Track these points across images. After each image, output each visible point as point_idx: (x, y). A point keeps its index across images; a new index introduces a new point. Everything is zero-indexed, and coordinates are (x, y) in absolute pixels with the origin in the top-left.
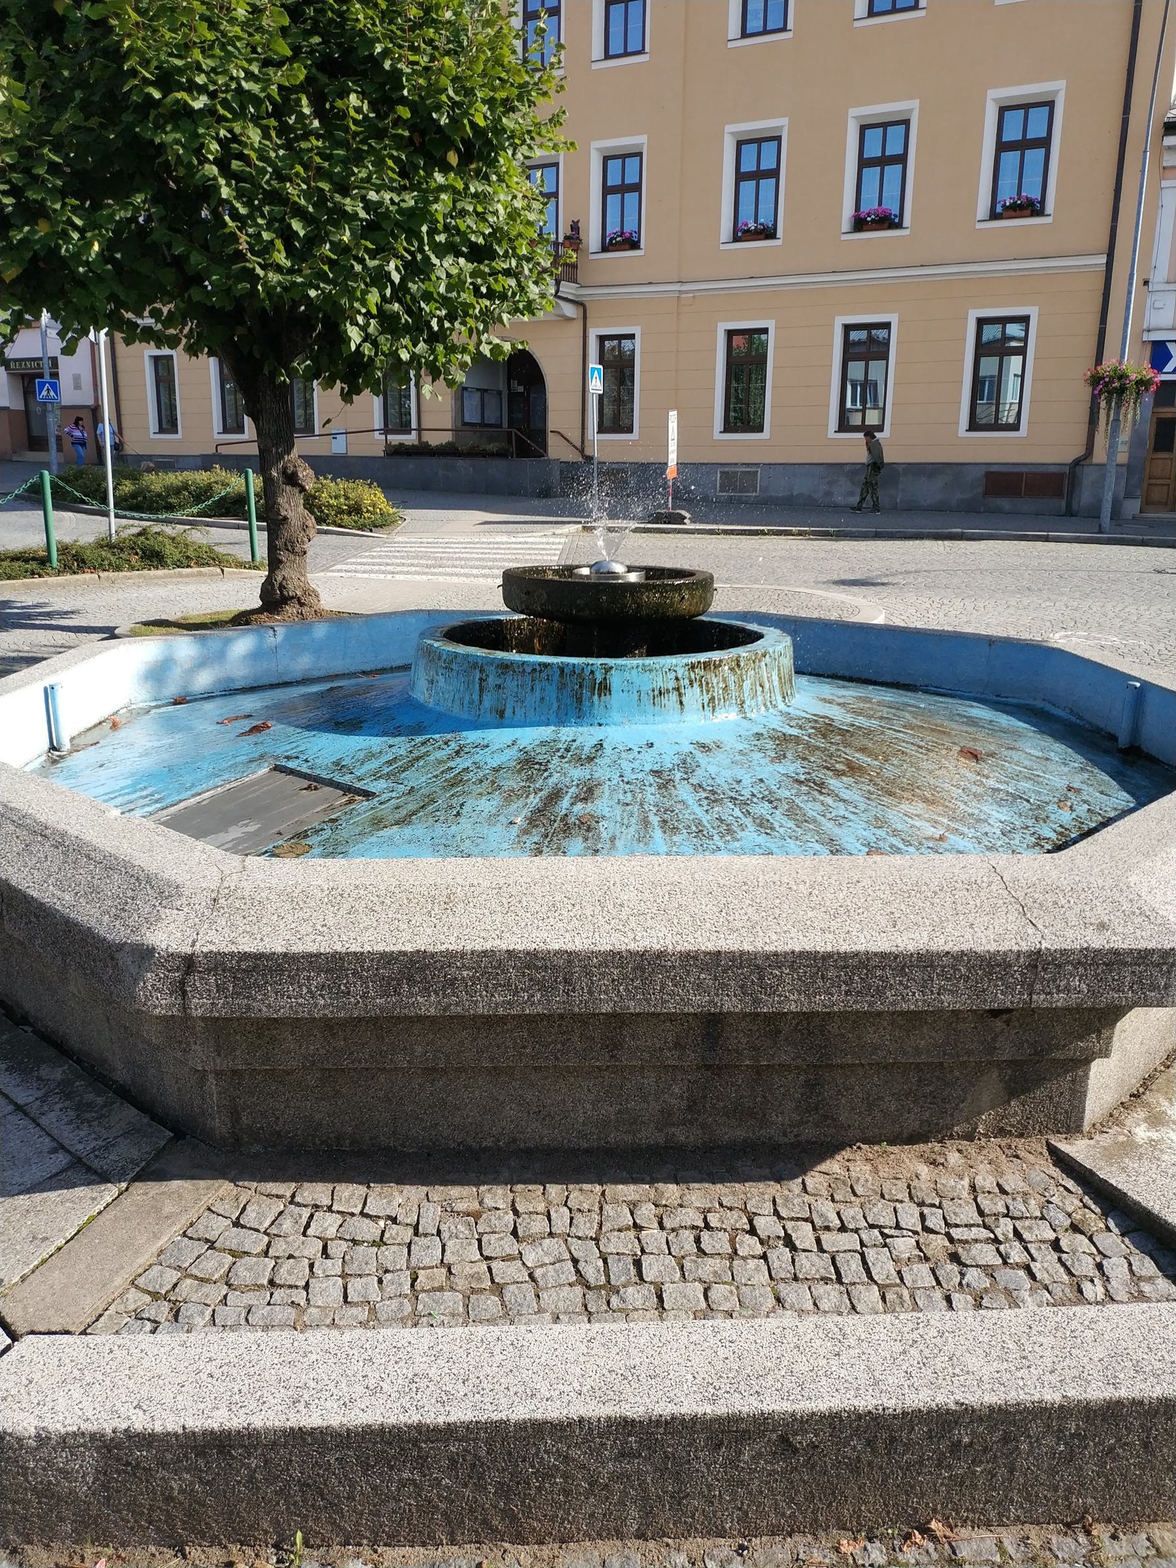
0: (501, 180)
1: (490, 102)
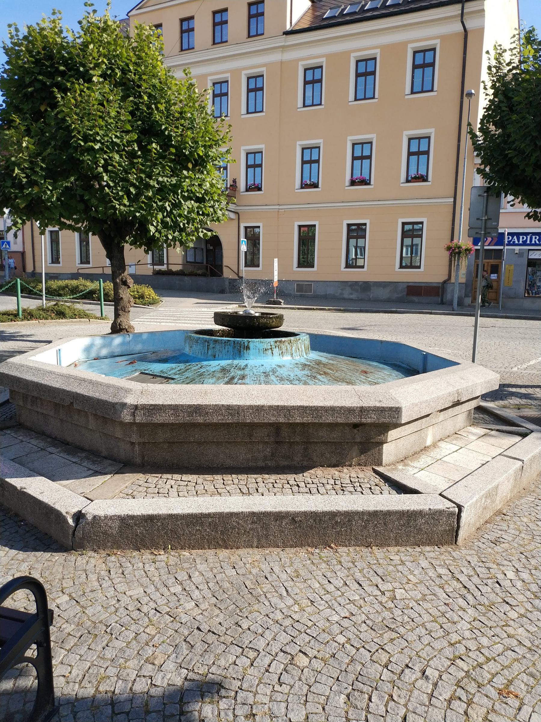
0: (208, 174)
1: (205, 146)
